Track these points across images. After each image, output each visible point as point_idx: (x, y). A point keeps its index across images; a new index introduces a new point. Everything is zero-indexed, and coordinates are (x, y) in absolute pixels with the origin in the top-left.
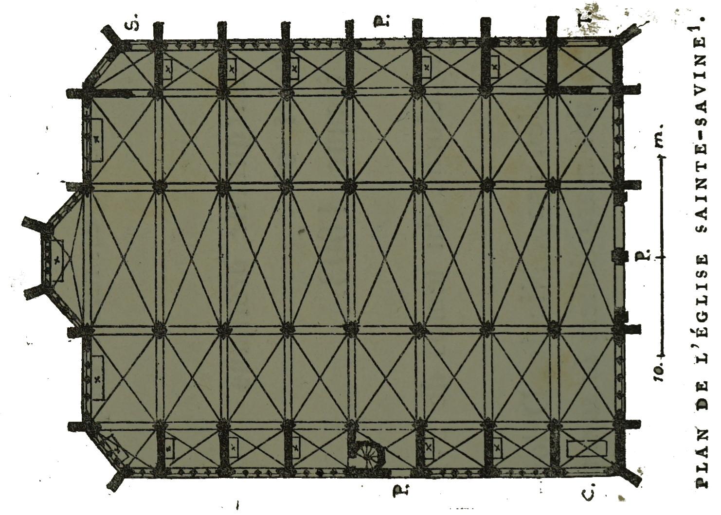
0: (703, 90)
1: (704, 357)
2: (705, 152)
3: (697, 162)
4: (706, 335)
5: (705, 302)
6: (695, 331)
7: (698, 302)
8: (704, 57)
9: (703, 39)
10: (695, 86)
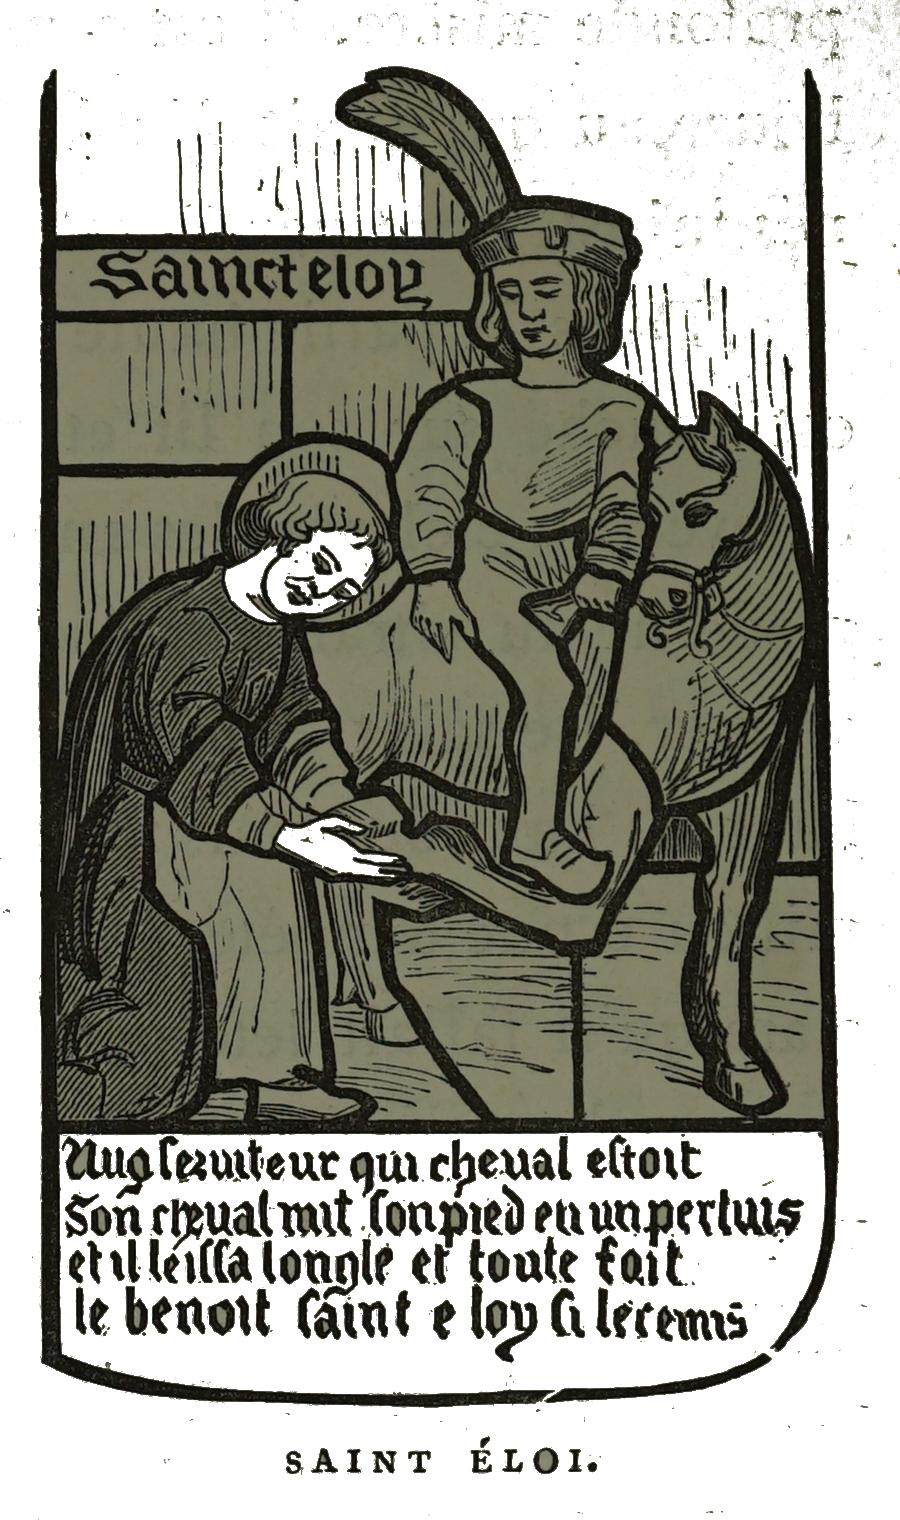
1: (515, 1465)
3: (428, 1454)
4: (476, 1469)
5: (509, 1468)
6: (486, 1448)
7: (510, 1453)
9: (489, 1469)
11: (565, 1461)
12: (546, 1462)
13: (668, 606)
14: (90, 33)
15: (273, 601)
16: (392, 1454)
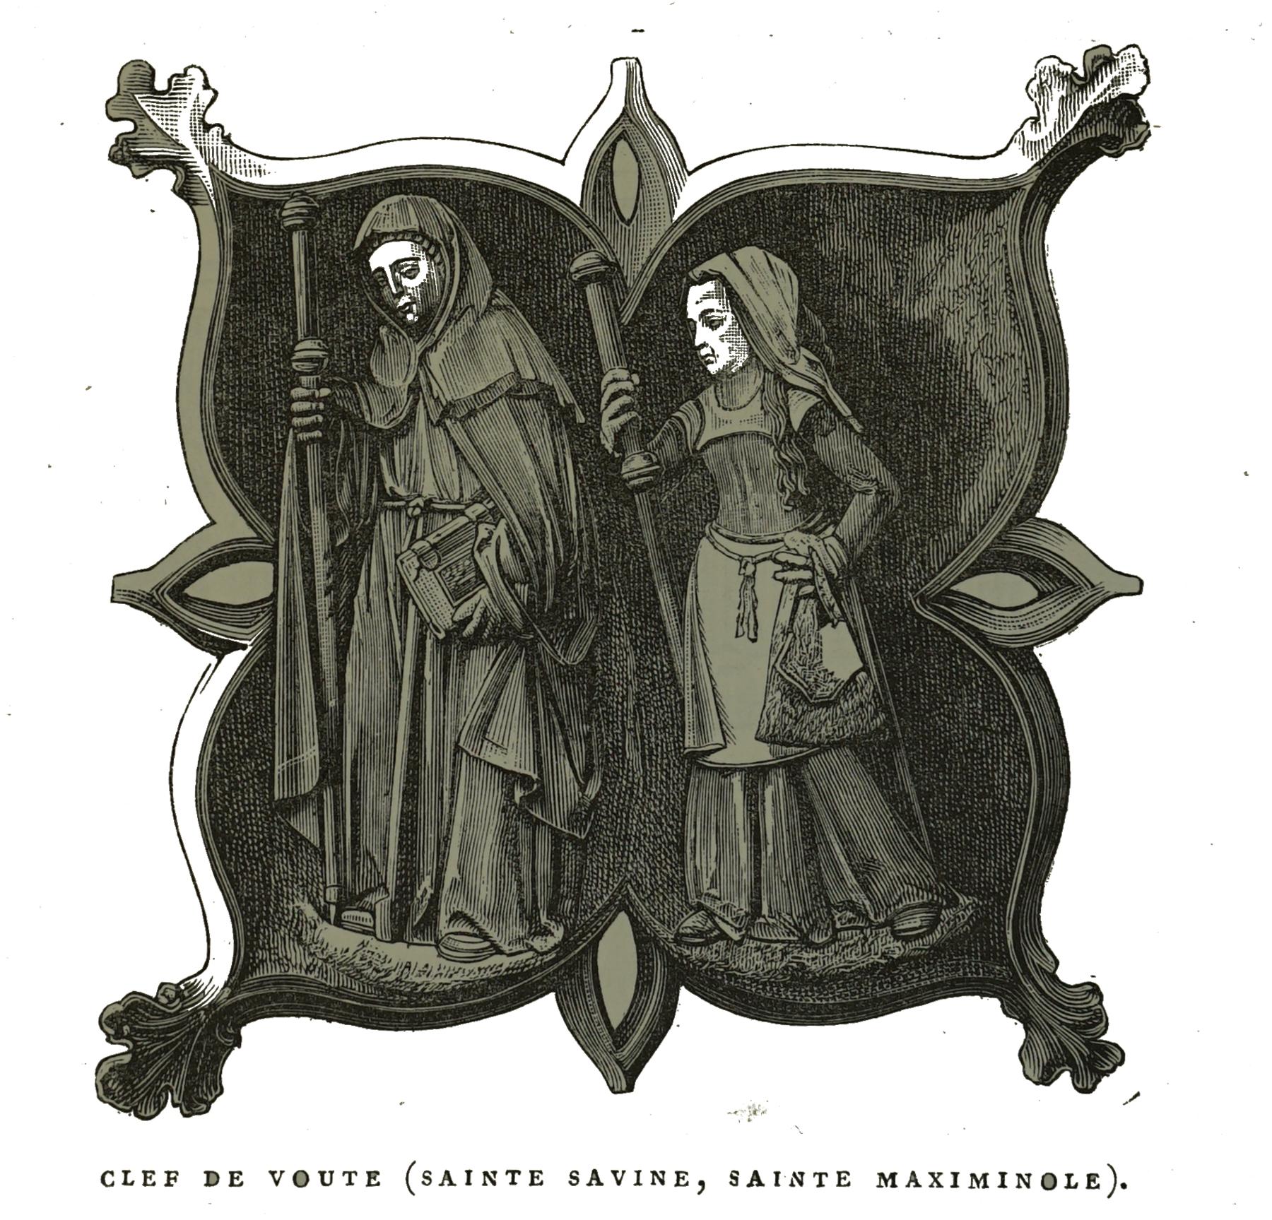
0: (619, 1183)
1: (1073, 1184)
2: (369, 1184)
4: (532, 1184)
5: (1069, 1186)
7: (1069, 1176)
8: (1028, 1185)
10: (282, 1172)
11: (1062, 1181)
12: (1049, 1183)
13: (127, 126)
14: (1246, 474)
15: (1047, 233)
16: (495, 1173)
